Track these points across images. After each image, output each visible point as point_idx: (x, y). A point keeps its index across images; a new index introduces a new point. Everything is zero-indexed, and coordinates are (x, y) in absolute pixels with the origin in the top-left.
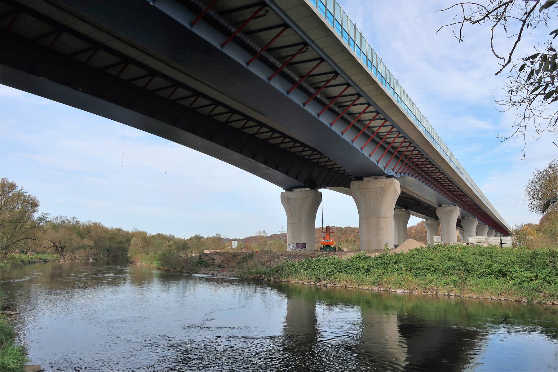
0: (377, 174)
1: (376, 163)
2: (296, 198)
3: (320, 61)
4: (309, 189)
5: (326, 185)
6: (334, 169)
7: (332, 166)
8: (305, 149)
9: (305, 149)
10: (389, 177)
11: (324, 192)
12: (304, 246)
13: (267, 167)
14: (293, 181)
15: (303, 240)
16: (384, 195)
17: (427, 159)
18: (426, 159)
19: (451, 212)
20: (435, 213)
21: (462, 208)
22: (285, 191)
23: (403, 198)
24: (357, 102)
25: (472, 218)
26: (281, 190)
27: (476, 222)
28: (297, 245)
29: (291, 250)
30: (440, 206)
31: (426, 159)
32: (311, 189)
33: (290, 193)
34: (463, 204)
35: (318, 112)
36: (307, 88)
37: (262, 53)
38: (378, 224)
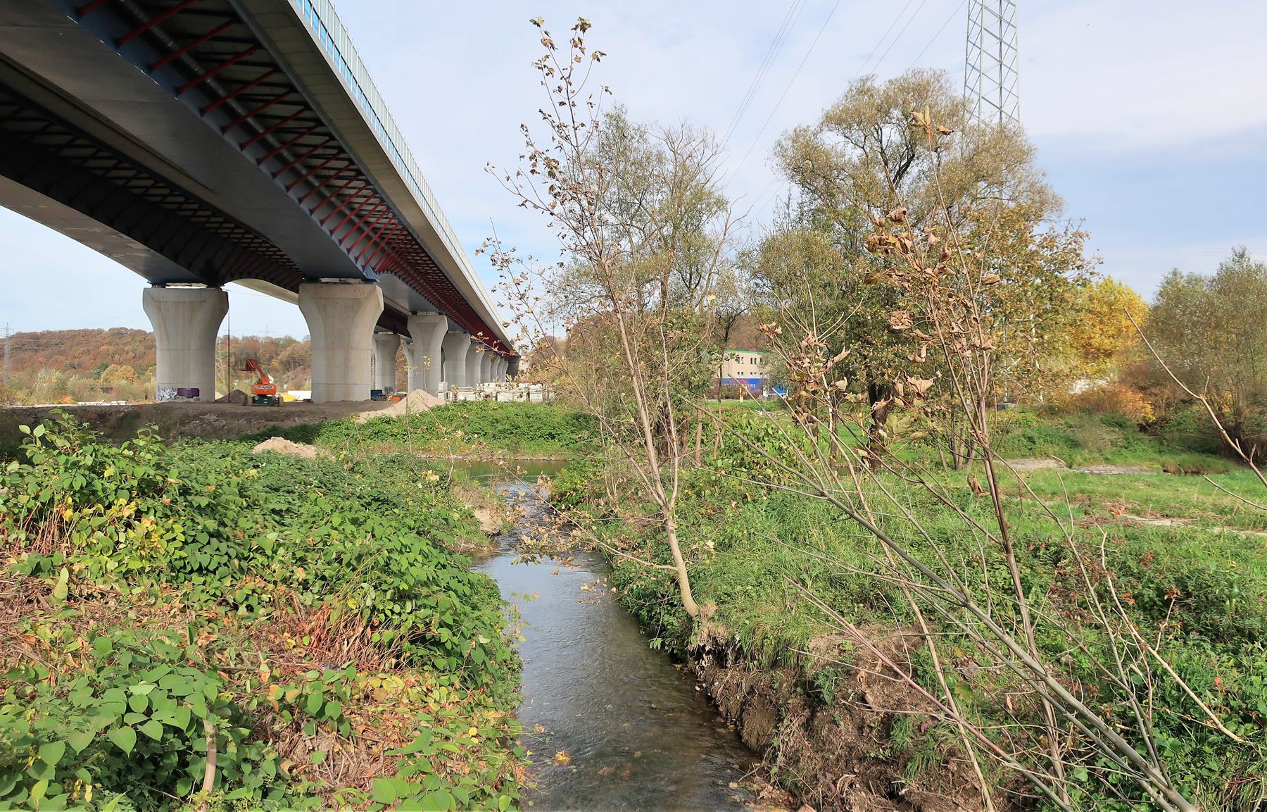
0: (347, 274)
1: (354, 261)
2: (178, 302)
3: (271, 69)
4: (204, 286)
5: (232, 278)
6: (150, 198)
7: (124, 181)
8: (78, 142)
9: (78, 142)
10: (367, 281)
11: (230, 287)
12: (195, 392)
13: (146, 247)
14: (169, 265)
15: (192, 382)
16: (358, 311)
17: (352, 163)
18: (347, 163)
19: (434, 326)
20: (406, 324)
21: (410, 285)
22: (150, 286)
23: (270, 255)
24: (285, 99)
25: (434, 313)
26: (144, 283)
27: (443, 326)
28: (180, 392)
29: (167, 401)
30: (414, 313)
31: (347, 163)
32: (209, 285)
33: (159, 290)
34: (418, 278)
35: (288, 184)
36: (189, 63)
37: (229, 100)
38: (347, 360)
